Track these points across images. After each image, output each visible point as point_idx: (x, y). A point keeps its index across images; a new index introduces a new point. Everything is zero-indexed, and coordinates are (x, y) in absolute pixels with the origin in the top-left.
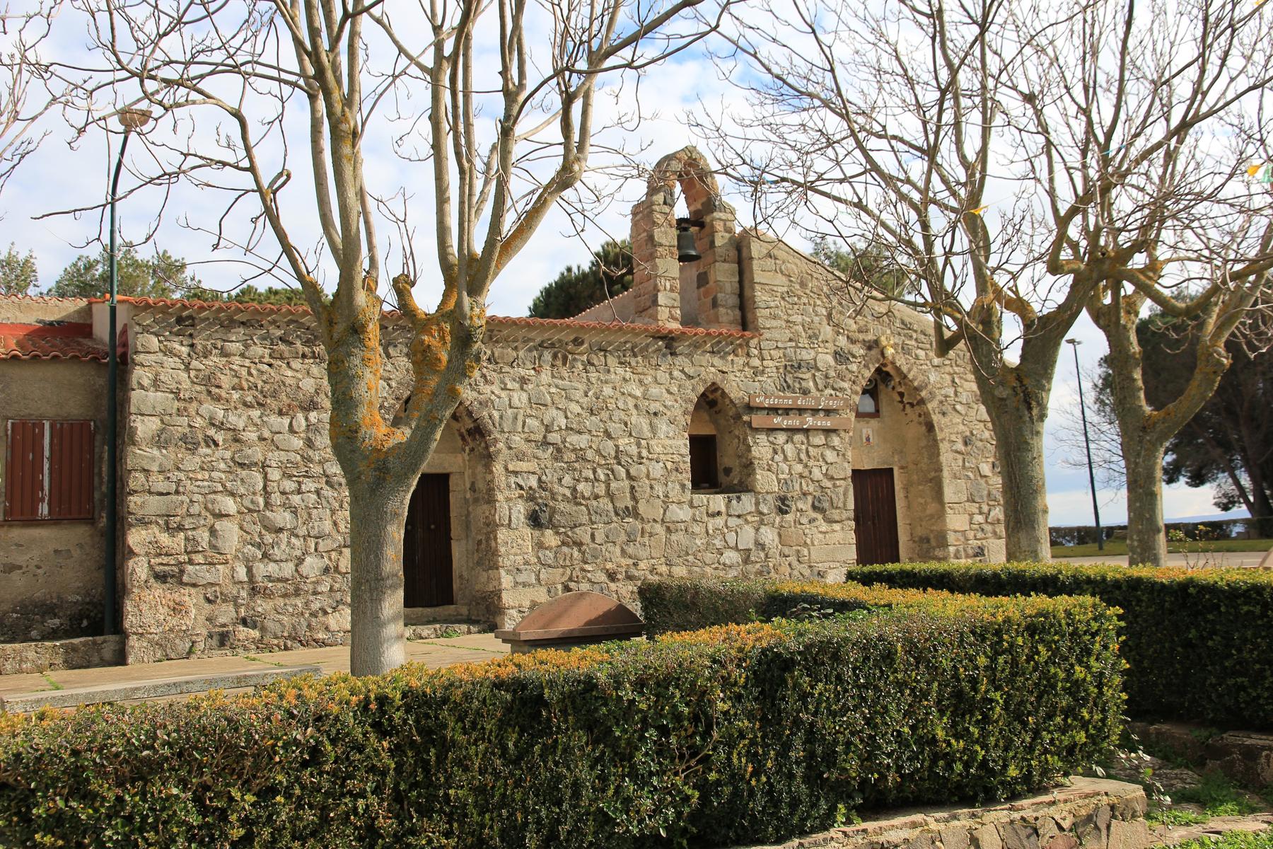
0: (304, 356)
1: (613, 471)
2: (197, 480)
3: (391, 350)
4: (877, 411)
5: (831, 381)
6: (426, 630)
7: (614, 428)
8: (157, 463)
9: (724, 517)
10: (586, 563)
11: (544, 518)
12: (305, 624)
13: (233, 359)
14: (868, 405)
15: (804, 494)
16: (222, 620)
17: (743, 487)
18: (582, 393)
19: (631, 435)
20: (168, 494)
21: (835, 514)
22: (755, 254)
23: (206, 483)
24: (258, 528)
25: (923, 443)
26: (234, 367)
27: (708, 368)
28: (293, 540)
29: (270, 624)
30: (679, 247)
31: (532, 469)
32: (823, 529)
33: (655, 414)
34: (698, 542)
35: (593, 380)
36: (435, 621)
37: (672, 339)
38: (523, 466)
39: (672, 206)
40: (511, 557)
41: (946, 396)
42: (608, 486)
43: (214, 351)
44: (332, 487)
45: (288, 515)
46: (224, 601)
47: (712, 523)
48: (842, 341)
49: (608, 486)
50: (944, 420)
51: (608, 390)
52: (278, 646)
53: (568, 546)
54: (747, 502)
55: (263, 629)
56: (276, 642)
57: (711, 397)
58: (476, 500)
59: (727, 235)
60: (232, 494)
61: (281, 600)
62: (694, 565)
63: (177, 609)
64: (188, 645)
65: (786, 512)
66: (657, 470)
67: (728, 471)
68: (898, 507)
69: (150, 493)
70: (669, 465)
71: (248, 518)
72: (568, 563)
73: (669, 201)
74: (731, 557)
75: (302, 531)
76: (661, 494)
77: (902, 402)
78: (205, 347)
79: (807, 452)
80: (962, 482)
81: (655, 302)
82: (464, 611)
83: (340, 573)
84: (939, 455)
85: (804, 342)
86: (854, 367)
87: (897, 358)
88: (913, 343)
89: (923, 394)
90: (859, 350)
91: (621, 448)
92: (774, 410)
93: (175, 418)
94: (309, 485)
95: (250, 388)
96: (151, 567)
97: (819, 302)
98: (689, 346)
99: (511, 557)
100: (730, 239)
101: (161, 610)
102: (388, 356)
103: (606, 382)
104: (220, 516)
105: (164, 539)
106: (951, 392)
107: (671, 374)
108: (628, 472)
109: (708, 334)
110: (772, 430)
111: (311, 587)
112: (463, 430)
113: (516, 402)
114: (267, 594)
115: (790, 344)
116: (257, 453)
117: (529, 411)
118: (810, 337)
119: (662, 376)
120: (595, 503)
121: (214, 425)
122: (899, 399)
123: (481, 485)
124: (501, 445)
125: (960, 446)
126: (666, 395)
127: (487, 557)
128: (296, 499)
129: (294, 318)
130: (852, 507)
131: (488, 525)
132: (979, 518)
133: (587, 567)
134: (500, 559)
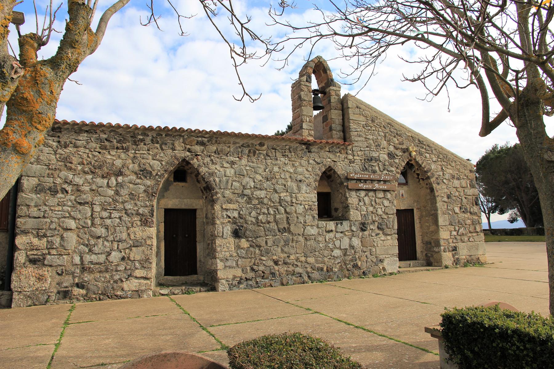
0: (117, 148)
1: (277, 209)
2: (55, 211)
3: (163, 147)
4: (407, 182)
6: (177, 290)
7: (279, 187)
8: (34, 202)
9: (334, 233)
10: (263, 256)
11: (241, 233)
12: (110, 287)
13: (80, 149)
14: (403, 180)
15: (374, 222)
16: (65, 285)
18: (262, 169)
19: (287, 191)
20: (39, 218)
21: (388, 231)
22: (350, 106)
23: (60, 213)
24: (87, 236)
25: (428, 197)
26: (80, 153)
27: (328, 159)
28: (106, 243)
29: (91, 287)
30: (314, 103)
31: (235, 208)
32: (382, 239)
33: (300, 181)
34: (321, 245)
35: (269, 164)
36: (182, 284)
37: (310, 144)
38: (231, 206)
39: (310, 82)
40: (223, 253)
41: (440, 176)
42: (275, 217)
43: (71, 145)
44: (128, 215)
45: (103, 230)
46: (67, 274)
48: (392, 148)
49: (275, 217)
50: (438, 187)
51: (276, 169)
52: (95, 298)
55: (88, 289)
56: (94, 296)
57: (328, 173)
58: (208, 223)
60: (74, 219)
63: (40, 278)
64: (45, 298)
65: (365, 230)
66: (300, 209)
67: (336, 210)
68: (416, 227)
69: (30, 217)
70: (307, 207)
71: (82, 231)
72: (253, 256)
73: (309, 80)
74: (337, 253)
75: (111, 238)
76: (302, 221)
77: (418, 178)
78: (65, 143)
79: (375, 201)
81: (301, 128)
82: (201, 278)
83: (130, 260)
84: (436, 203)
85: (373, 148)
86: (397, 161)
87: (417, 157)
88: (424, 150)
89: (429, 174)
90: (399, 153)
91: (282, 198)
92: (359, 180)
93: (46, 178)
94: (115, 214)
95: (88, 164)
96: (27, 256)
97: (380, 130)
99: (223, 253)
100: (338, 99)
101: (32, 279)
102: (162, 149)
104: (67, 229)
105: (35, 241)
106: (441, 173)
107: (308, 161)
109: (327, 143)
110: (358, 190)
111: (114, 267)
112: (202, 188)
114: (91, 271)
115: (367, 149)
116: (88, 197)
117: (234, 178)
118: (376, 146)
119: (304, 162)
120: (268, 226)
121: (67, 182)
123: (210, 216)
124: (219, 195)
125: (445, 199)
126: (306, 172)
127: (212, 252)
128: (108, 222)
129: (114, 129)
130: (397, 228)
131: (212, 236)
132: (454, 233)
133: (263, 258)
134: (217, 254)
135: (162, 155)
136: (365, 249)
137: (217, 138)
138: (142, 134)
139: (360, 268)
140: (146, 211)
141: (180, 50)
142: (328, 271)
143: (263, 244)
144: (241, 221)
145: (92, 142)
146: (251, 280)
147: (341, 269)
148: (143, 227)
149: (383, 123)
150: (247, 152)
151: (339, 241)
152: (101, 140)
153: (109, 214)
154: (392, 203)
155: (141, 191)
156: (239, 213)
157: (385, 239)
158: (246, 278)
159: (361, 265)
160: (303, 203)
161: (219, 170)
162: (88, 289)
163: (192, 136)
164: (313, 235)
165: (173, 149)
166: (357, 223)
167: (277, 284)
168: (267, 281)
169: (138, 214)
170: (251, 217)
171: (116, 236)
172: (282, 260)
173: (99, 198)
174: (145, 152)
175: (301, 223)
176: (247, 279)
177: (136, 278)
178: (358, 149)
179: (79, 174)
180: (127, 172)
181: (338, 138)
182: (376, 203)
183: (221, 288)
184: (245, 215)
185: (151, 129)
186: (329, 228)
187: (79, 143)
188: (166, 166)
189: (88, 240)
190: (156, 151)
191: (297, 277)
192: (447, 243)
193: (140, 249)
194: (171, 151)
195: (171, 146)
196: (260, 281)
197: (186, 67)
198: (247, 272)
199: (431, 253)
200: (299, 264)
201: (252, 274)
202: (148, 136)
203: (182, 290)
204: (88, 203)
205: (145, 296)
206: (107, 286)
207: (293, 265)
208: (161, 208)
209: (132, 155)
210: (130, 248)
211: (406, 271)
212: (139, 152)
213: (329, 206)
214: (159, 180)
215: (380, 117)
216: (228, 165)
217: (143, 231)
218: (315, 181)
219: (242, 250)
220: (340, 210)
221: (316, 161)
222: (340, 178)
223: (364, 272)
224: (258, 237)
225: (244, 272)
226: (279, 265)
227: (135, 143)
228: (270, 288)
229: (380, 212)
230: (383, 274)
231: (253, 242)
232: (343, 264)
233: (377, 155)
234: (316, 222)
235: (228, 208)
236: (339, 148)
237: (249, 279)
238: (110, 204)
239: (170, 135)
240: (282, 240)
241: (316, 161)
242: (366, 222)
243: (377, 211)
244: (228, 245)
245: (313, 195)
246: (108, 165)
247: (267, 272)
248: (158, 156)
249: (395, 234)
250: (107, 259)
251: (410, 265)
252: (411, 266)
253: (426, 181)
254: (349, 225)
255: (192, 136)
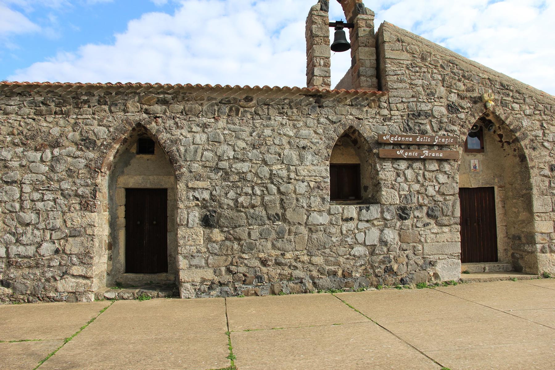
0: (56, 113)
1: (267, 189)
3: (112, 108)
4: (483, 148)
5: (444, 125)
6: (126, 293)
10: (244, 253)
13: (11, 116)
15: (421, 206)
17: (375, 200)
18: (248, 133)
19: (283, 163)
21: (445, 220)
24: (15, 223)
25: (517, 169)
26: (11, 121)
27: (348, 116)
28: (36, 232)
29: (18, 286)
31: (205, 187)
32: (435, 231)
33: (304, 148)
34: (334, 239)
35: (258, 125)
37: (321, 96)
38: (200, 184)
40: (188, 247)
42: (263, 199)
44: (64, 197)
45: (33, 216)
47: (346, 226)
48: (454, 98)
49: (263, 199)
50: (533, 153)
51: (267, 132)
52: (23, 300)
53: (230, 241)
54: (374, 211)
55: (14, 289)
56: (22, 297)
59: (368, 29)
61: (27, 270)
62: (329, 255)
65: (406, 219)
66: (302, 188)
67: (366, 188)
68: (497, 214)
70: (312, 184)
71: (8, 217)
72: (229, 252)
73: (324, 7)
74: (359, 250)
75: (42, 225)
76: (305, 205)
77: (501, 141)
79: (424, 175)
80: (548, 198)
83: (66, 254)
84: (529, 178)
85: (423, 97)
86: (462, 116)
87: (497, 109)
88: (510, 99)
89: (518, 134)
90: (466, 104)
91: (274, 172)
92: (398, 145)
94: (49, 196)
95: (19, 134)
97: (435, 71)
98: (333, 101)
102: (111, 112)
103: (267, 126)
106: (540, 133)
107: (318, 120)
108: (279, 189)
111: (46, 262)
113: (198, 140)
114: (18, 266)
115: (412, 100)
116: (17, 175)
117: (206, 146)
120: (252, 211)
122: (499, 139)
124: (184, 170)
125: (547, 172)
126: (314, 135)
128: (40, 205)
134: (179, 248)
135: (110, 119)
136: (405, 246)
137: (185, 93)
138: (86, 94)
139: (396, 274)
140: (87, 192)
141: (283, 32)
142: (344, 276)
143: (245, 236)
144: (213, 204)
145: (25, 106)
146: (227, 285)
147: (366, 274)
148: (82, 212)
149: (440, 62)
150: (227, 111)
151: (363, 234)
152: (36, 103)
153: (41, 195)
154: (453, 178)
155: (82, 165)
156: (211, 193)
157: (440, 231)
158: (219, 282)
159: (398, 268)
160: (307, 178)
161: (185, 136)
162: (14, 289)
163: (151, 92)
164: (321, 225)
165: (125, 111)
166: (392, 208)
167: (266, 292)
168: (250, 287)
169: (77, 195)
170: (227, 198)
171: (49, 223)
172: (273, 259)
173: (30, 175)
174: (89, 117)
175: (303, 207)
176: (221, 284)
177: (73, 276)
178: (399, 100)
179: (8, 147)
180: (66, 143)
181: (370, 87)
182: (425, 179)
183: (184, 293)
184: (220, 196)
185: (99, 87)
186: (346, 215)
187: (9, 108)
188: (115, 133)
189: (16, 228)
190: (103, 114)
191: (296, 283)
192: (548, 239)
193: (78, 239)
194: (122, 113)
195: (122, 107)
196: (241, 287)
197: (289, 50)
198: (220, 274)
199: (521, 253)
200: (299, 265)
201: (228, 277)
202: (94, 96)
203: (133, 294)
204: (16, 182)
205: (84, 300)
206: (38, 286)
207: (290, 267)
208: (120, 188)
209: (73, 121)
210: (66, 238)
211: (474, 280)
212: (81, 117)
213: (350, 183)
214: (105, 151)
215: (436, 53)
216: (199, 129)
217: (82, 217)
218: (327, 147)
219: (214, 245)
220: (370, 189)
221: (329, 120)
222: (367, 142)
223: (402, 280)
224: (236, 227)
225: (217, 273)
226: (269, 265)
227: (77, 106)
228: (254, 297)
229: (431, 191)
230: (434, 283)
231: (230, 234)
232: (369, 266)
233: (429, 108)
234: (327, 206)
235: (196, 186)
236: (367, 99)
237: (224, 284)
238: (42, 183)
239: (122, 93)
240: (273, 232)
241: (329, 120)
242: (408, 206)
243: (426, 190)
244: (194, 236)
245: (323, 168)
246: (43, 134)
247: (250, 275)
248: (105, 121)
249: (456, 224)
250: (37, 251)
251: (484, 269)
252: (487, 270)
253: (513, 146)
254: (379, 210)
255: (151, 92)
